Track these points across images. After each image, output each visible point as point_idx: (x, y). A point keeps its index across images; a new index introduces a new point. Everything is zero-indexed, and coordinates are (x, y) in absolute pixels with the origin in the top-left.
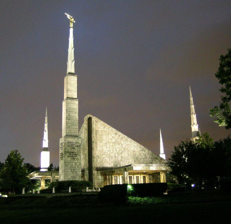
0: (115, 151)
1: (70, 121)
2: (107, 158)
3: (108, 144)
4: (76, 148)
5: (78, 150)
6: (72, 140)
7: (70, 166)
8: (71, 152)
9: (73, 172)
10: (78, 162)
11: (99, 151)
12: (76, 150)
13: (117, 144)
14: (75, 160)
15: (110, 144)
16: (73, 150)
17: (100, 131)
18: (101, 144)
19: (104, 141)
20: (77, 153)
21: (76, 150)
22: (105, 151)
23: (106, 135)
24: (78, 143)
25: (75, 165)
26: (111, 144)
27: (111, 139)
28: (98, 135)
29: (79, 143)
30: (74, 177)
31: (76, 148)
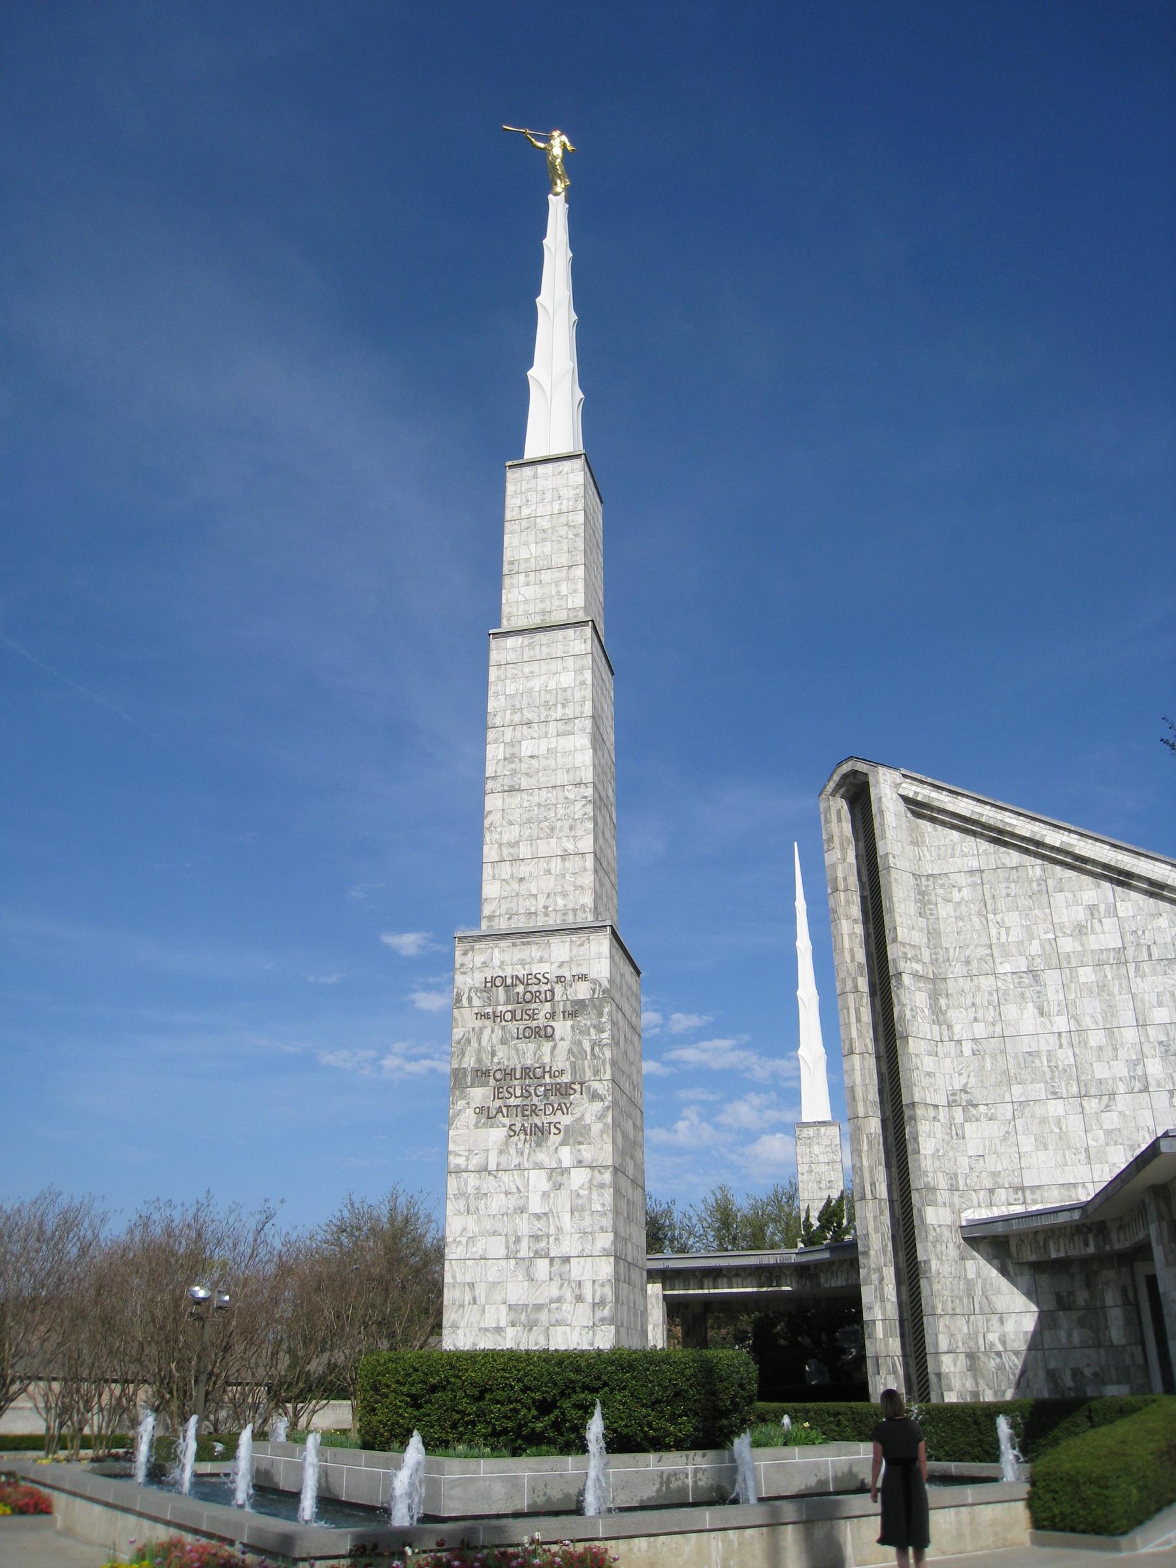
0: (1130, 1035)
1: (516, 799)
2: (1056, 1108)
3: (1052, 978)
4: (562, 1028)
5: (579, 1043)
6: (523, 963)
7: (497, 1203)
8: (509, 1073)
9: (527, 1264)
10: (580, 1163)
11: (967, 1048)
12: (563, 1047)
13: (1146, 967)
14: (554, 1139)
15: (1074, 978)
16: (529, 1053)
17: (962, 880)
18: (987, 983)
19: (1007, 955)
20: (566, 1078)
21: (563, 1047)
22: (1026, 1045)
23: (1024, 902)
24: (583, 977)
25: (545, 1195)
26: (1087, 975)
27: (1080, 930)
28: (944, 911)
29: (595, 982)
30: (538, 1308)
31: (562, 1028)
